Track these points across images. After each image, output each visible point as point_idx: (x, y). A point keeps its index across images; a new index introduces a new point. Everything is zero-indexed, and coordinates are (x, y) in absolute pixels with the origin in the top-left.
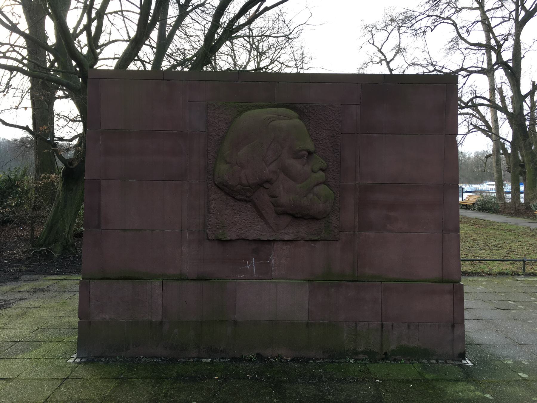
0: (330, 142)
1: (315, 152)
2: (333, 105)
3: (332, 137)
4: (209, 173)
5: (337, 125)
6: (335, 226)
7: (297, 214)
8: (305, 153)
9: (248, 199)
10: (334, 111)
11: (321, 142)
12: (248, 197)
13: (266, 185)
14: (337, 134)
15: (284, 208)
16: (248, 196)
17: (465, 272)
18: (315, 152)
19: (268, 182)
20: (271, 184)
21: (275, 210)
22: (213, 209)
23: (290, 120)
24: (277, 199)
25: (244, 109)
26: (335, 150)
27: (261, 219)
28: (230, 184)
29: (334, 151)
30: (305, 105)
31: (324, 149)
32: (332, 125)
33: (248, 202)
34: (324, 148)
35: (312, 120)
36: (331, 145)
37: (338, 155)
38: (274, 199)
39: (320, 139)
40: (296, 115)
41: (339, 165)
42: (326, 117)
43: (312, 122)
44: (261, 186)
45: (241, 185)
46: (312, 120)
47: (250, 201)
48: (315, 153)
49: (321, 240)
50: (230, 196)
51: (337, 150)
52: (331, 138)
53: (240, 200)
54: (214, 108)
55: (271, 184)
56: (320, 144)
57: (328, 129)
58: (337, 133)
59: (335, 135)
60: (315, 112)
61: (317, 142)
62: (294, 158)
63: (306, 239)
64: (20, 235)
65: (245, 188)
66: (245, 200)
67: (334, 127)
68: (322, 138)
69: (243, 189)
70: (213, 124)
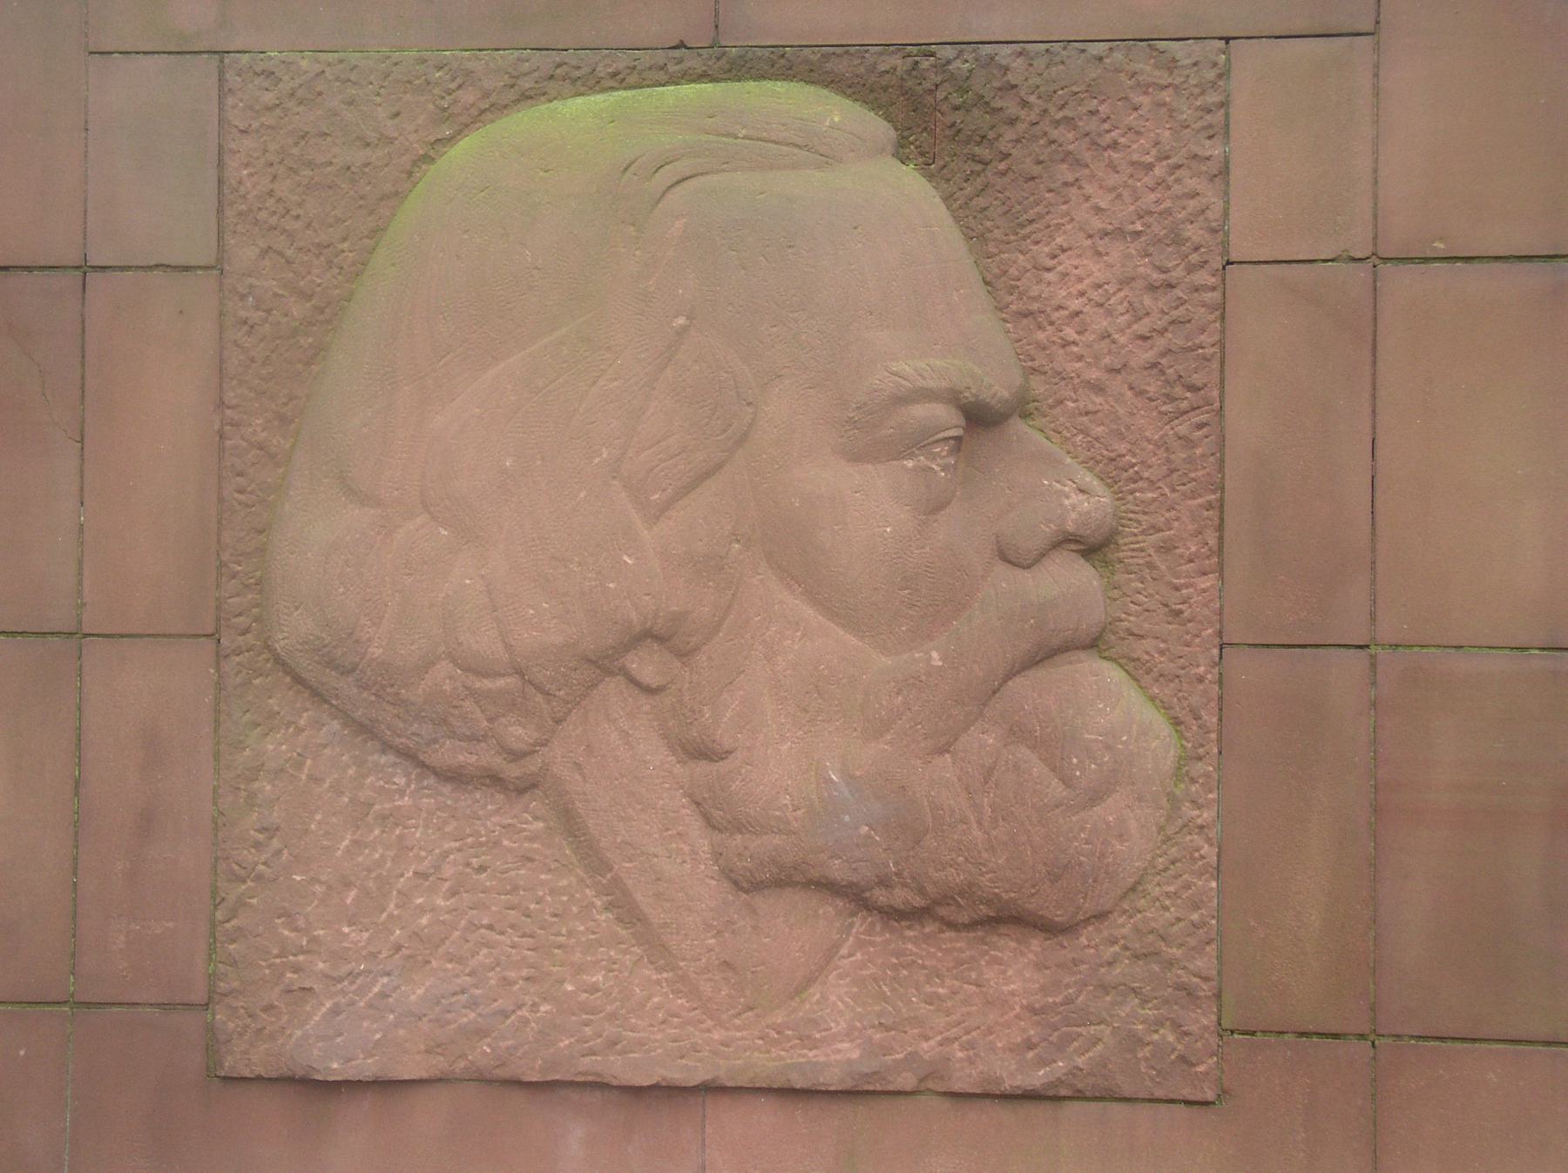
0: (1142, 327)
1: (1022, 407)
2: (1161, 45)
3: (1152, 288)
4: (234, 576)
5: (1194, 195)
6: (1180, 987)
7: (884, 882)
8: (947, 417)
9: (512, 771)
10: (1166, 96)
11: (1070, 333)
12: (516, 756)
13: (647, 665)
14: (1191, 269)
15: (777, 840)
16: (516, 746)
17: (305, 680)
18: (1022, 407)
19: (660, 639)
20: (684, 655)
21: (717, 855)
22: (257, 845)
23: (819, 167)
24: (722, 767)
25: (486, 95)
26: (1178, 390)
27: (619, 920)
28: (376, 651)
29: (1171, 399)
30: (948, 52)
31: (1098, 388)
32: (1152, 197)
33: (520, 791)
34: (1094, 374)
35: (1002, 166)
36: (1149, 356)
37: (1200, 426)
38: (702, 767)
39: (1060, 307)
40: (877, 127)
41: (1209, 506)
42: (1108, 138)
43: (1000, 182)
44: (611, 673)
45: (454, 662)
46: (1002, 166)
47: (525, 787)
48: (1026, 415)
49: (1079, 1096)
50: (386, 747)
51: (1193, 388)
52: (1147, 301)
53: (455, 777)
54: (269, 98)
55: (684, 655)
56: (1066, 344)
57: (1118, 233)
58: (1194, 258)
59: (1179, 273)
60: (1025, 104)
61: (1040, 336)
62: (857, 457)
63: (957, 1087)
64: (750, 421)
65: (488, 684)
66: (494, 780)
67: (1168, 212)
68: (1075, 304)
69: (473, 693)
70: (263, 215)
